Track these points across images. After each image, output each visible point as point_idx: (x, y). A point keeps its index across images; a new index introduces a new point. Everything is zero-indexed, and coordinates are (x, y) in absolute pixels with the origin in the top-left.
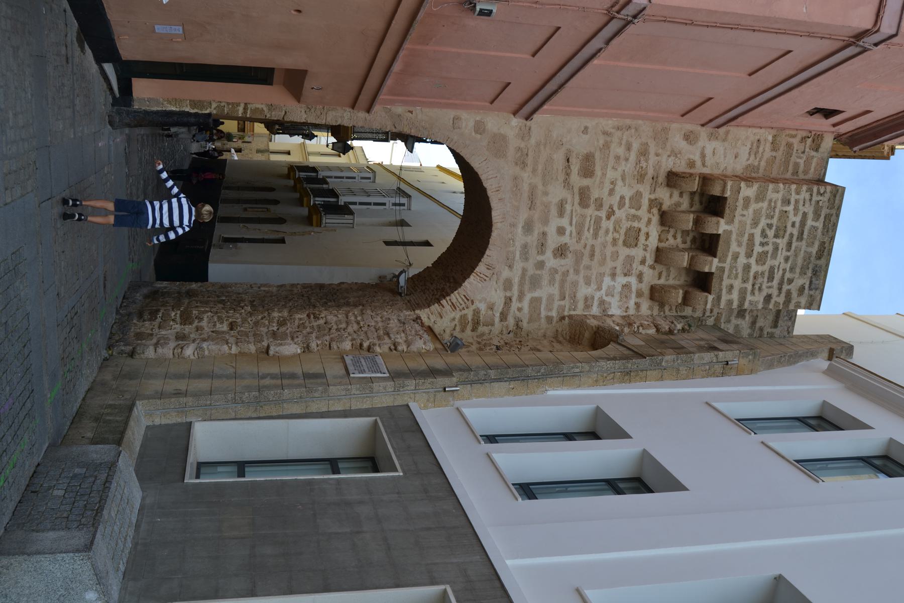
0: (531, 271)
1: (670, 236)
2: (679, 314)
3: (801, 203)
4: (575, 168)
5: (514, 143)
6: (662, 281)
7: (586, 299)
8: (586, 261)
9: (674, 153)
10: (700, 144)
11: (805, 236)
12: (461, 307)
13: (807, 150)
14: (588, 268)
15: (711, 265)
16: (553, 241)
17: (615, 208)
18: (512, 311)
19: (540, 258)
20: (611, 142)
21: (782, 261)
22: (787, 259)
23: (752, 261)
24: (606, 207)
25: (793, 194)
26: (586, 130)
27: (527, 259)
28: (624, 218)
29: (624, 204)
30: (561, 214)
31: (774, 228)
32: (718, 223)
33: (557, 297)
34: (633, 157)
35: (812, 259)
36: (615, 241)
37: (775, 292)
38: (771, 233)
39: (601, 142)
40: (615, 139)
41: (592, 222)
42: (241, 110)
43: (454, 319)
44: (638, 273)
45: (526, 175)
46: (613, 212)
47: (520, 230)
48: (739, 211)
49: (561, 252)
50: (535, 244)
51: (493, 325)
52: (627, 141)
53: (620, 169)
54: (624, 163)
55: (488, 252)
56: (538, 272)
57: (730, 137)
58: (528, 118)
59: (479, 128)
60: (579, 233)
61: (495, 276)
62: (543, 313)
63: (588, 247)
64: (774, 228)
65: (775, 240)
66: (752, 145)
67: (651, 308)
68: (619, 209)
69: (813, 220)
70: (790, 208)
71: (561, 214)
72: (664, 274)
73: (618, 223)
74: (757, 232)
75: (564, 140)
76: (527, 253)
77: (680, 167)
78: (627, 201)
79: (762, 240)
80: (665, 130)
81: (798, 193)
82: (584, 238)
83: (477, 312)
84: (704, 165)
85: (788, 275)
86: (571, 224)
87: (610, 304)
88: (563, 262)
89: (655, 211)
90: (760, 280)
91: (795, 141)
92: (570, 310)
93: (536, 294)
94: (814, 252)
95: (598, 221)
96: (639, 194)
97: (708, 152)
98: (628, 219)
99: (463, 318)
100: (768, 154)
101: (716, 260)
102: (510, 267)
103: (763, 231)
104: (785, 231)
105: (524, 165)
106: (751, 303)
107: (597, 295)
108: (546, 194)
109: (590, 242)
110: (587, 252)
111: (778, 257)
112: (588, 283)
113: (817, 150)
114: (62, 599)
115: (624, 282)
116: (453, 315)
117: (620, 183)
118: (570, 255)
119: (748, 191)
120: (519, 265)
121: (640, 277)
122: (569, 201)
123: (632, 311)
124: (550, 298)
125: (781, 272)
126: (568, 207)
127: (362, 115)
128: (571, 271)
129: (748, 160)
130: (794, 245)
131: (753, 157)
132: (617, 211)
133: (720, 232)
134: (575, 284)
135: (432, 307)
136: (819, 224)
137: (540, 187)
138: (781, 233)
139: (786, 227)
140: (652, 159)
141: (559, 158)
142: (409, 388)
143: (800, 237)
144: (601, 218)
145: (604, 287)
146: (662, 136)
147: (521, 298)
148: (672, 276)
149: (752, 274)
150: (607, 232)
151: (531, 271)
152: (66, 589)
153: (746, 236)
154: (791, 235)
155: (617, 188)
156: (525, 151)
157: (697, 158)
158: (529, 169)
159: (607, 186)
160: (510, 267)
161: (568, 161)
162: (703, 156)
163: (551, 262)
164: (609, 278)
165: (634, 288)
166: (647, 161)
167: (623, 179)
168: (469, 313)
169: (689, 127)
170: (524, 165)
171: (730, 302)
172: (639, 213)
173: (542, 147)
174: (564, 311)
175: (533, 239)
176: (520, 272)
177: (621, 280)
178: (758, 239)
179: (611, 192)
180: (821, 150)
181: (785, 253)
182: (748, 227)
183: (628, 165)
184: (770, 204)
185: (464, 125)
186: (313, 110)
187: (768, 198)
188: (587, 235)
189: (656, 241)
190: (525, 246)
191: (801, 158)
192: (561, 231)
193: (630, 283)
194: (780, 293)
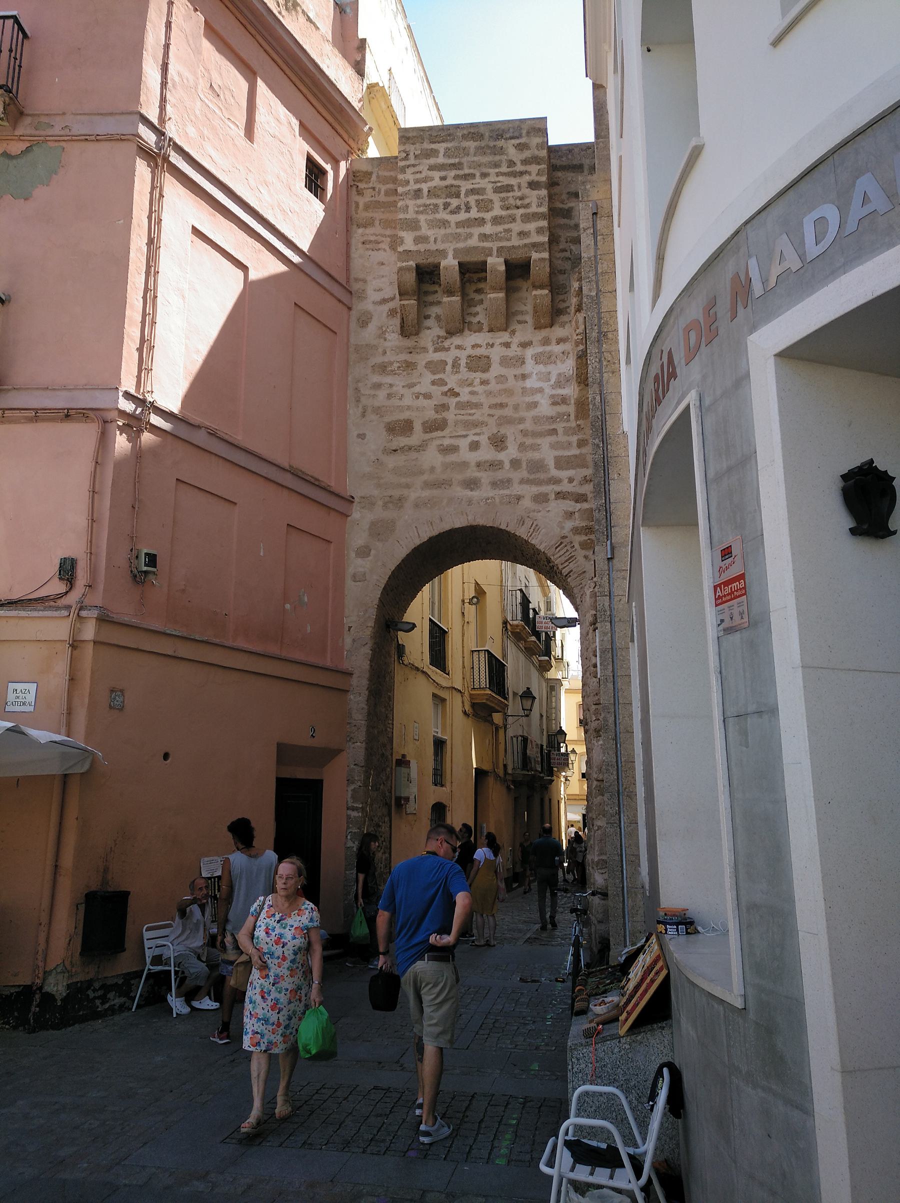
0: (524, 473)
1: (475, 320)
3: (418, 176)
4: (403, 441)
5: (379, 513)
6: (529, 318)
7: (554, 404)
8: (508, 412)
9: (382, 335)
10: (370, 307)
11: (457, 160)
13: (371, 185)
14: (516, 408)
15: (496, 263)
16: (486, 453)
17: (446, 389)
21: (487, 180)
22: (484, 175)
24: (445, 400)
25: (408, 188)
27: (509, 481)
31: (448, 200)
32: (446, 268)
33: (553, 439)
34: (388, 380)
35: (483, 144)
36: (484, 382)
37: (527, 178)
38: (454, 202)
39: (373, 417)
41: (462, 412)
42: (354, 814)
44: (520, 348)
45: (413, 495)
46: (451, 390)
47: (475, 493)
48: (433, 247)
49: (499, 442)
50: (490, 473)
54: (394, 388)
55: (503, 527)
57: (361, 276)
58: (350, 500)
59: (364, 552)
60: (475, 425)
61: (531, 514)
62: (575, 451)
64: (448, 200)
65: (462, 196)
70: (425, 187)
71: (454, 449)
72: (520, 318)
74: (453, 219)
75: (373, 458)
76: (502, 481)
78: (437, 377)
79: (463, 211)
81: (407, 182)
82: (481, 419)
83: (576, 531)
84: (392, 299)
86: (465, 436)
87: (560, 374)
89: (447, 344)
90: (512, 201)
92: (568, 421)
93: (551, 463)
94: (476, 144)
95: (460, 406)
96: (430, 365)
97: (377, 297)
100: (377, 229)
101: (490, 260)
102: (519, 498)
103: (452, 212)
104: (452, 186)
106: (539, 205)
107: (548, 391)
109: (486, 410)
110: (498, 412)
111: (483, 186)
112: (535, 405)
115: (533, 362)
116: (581, 559)
117: (417, 389)
118: (503, 431)
119: (408, 241)
120: (517, 489)
121: (524, 345)
122: (439, 442)
123: (567, 347)
124: (553, 446)
125: (501, 178)
126: (447, 442)
127: (354, 681)
128: (521, 427)
129: (385, 250)
130: (467, 171)
131: (382, 246)
132: (449, 386)
133: (455, 263)
134: (536, 420)
136: (441, 147)
137: (425, 477)
138: (453, 189)
139: (446, 187)
140: (390, 357)
141: (392, 461)
144: (458, 403)
147: (558, 481)
148: (523, 308)
149: (504, 213)
150: (472, 393)
151: (524, 473)
153: (458, 230)
154: (456, 177)
158: (405, 492)
159: (422, 402)
160: (519, 498)
161: (395, 451)
163: (512, 451)
164: (527, 381)
165: (540, 349)
166: (391, 363)
167: (411, 386)
168: (578, 539)
171: (540, 231)
172: (450, 362)
175: (485, 477)
176: (526, 487)
177: (530, 366)
178: (463, 216)
179: (428, 396)
180: (370, 170)
181: (478, 179)
182: (449, 231)
183: (397, 383)
184: (422, 212)
186: (352, 735)
187: (415, 216)
188: (478, 415)
189: (482, 334)
190: (494, 484)
192: (475, 446)
194: (526, 172)
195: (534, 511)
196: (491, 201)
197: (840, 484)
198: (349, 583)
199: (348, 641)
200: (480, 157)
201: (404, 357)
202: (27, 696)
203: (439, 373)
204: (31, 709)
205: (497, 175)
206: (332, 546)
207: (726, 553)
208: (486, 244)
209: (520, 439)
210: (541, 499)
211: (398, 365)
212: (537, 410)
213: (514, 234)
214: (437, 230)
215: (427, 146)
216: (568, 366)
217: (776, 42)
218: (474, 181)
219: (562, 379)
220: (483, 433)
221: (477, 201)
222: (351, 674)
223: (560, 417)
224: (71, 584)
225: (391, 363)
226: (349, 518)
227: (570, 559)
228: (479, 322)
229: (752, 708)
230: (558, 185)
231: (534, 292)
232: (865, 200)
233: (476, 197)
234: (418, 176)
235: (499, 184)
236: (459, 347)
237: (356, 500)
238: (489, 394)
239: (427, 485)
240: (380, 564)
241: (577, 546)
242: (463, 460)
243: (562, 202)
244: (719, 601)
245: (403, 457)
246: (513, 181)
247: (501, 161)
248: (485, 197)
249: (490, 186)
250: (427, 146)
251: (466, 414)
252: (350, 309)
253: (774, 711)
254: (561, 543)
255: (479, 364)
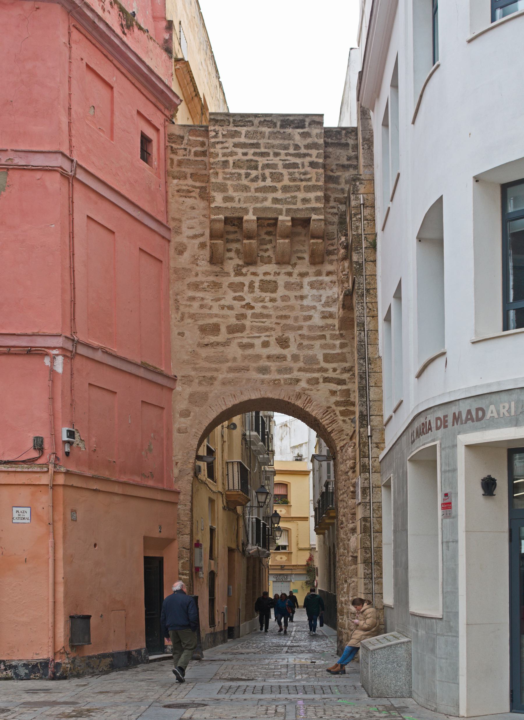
1: (266, 254)
2: (336, 236)
3: (225, 151)
4: (213, 339)
5: (195, 387)
6: (306, 256)
7: (324, 317)
8: (290, 322)
9: (195, 260)
10: (185, 241)
11: (255, 141)
12: (333, 416)
13: (183, 146)
14: (296, 319)
16: (275, 350)
17: (244, 303)
18: (336, 376)
19: (289, 358)
20: (189, 313)
21: (278, 158)
22: (276, 154)
23: (279, 185)
24: (244, 311)
26: (181, 334)
28: (252, 295)
29: (240, 296)
30: (252, 346)
31: (249, 171)
32: (247, 221)
33: (323, 342)
35: (275, 130)
36: (272, 300)
37: (308, 159)
38: (254, 173)
39: (190, 321)
40: (187, 310)
41: (256, 320)
43: (344, 421)
45: (221, 377)
48: (235, 205)
49: (283, 343)
50: (278, 364)
51: (348, 390)
52: (187, 300)
53: (211, 304)
56: (302, 359)
57: (177, 217)
58: (174, 379)
59: (186, 414)
60: (267, 329)
61: (306, 392)
62: (338, 351)
63: (278, 321)
64: (249, 171)
65: (260, 168)
66: (181, 196)
67: (331, 262)
68: (244, 300)
69: (240, 137)
70: (231, 160)
71: (252, 346)
73: (256, 300)
74: (254, 186)
75: (190, 350)
77: (206, 253)
79: (260, 180)
80: (176, 270)
82: (270, 326)
83: (337, 404)
84: (202, 235)
85: (291, 151)
86: (259, 337)
87: (328, 297)
88: (292, 340)
89: (244, 270)
90: (297, 176)
91: (176, 158)
92: (334, 330)
93: (320, 358)
94: (270, 130)
95: (254, 316)
96: (231, 285)
97: (191, 233)
98: (253, 292)
99: (342, 413)
101: (280, 218)
102: (298, 381)
103: (253, 180)
105: (213, 378)
107: (320, 308)
108: (235, 359)
110: (283, 322)
113: (182, 138)
114: (399, 665)
115: (309, 287)
116: (341, 422)
117: (222, 302)
118: (286, 335)
120: (296, 374)
121: (302, 275)
122: (240, 341)
123: (334, 278)
124: (323, 347)
125: (289, 158)
126: (245, 341)
127: (181, 497)
129: (195, 198)
130: (263, 150)
131: (193, 194)
133: (255, 218)
134: (311, 328)
135: (334, 438)
136: (243, 130)
137: (229, 364)
138: (253, 164)
139: (247, 161)
141: (204, 352)
142: (367, 462)
143: (256, 145)
144: (253, 314)
145: (312, 304)
146: (181, 273)
147: (326, 370)
149: (292, 184)
150: (264, 307)
151: (301, 364)
152: (394, 662)
153: (257, 194)
154: (255, 154)
155: (227, 303)
156: (201, 378)
157: (197, 242)
158: (215, 374)
159: (226, 312)
160: (298, 381)
161: (207, 345)
162: (195, 237)
163: (293, 349)
165: (314, 279)
166: (202, 283)
167: (219, 299)
169: (172, 252)
170: (213, 378)
171: (317, 199)
172: (247, 284)
173: (197, 366)
174: (335, 335)
175: (273, 365)
177: (306, 290)
178: (261, 184)
179: (230, 308)
180: (182, 135)
181: (271, 157)
182: (249, 194)
183: (207, 297)
184: (228, 179)
185: (183, 425)
186: (181, 530)
187: (223, 181)
188: (268, 323)
189: (271, 265)
191: (190, 151)
193: (308, 283)
195: (308, 389)
196: (282, 174)
197: (481, 481)
198: (175, 435)
199: (176, 471)
200: (273, 141)
201: (212, 278)
202: (25, 514)
203: (239, 291)
204: (29, 521)
205: (287, 155)
206: (165, 411)
207: (446, 495)
208: (279, 206)
209: (299, 340)
210: (314, 382)
211: (207, 284)
212: (311, 321)
213: (299, 200)
214: (240, 193)
215: (232, 128)
216: (336, 292)
217: (473, 343)
218: (268, 158)
219: (330, 300)
220: (272, 336)
221: (271, 173)
222: (179, 493)
223: (327, 326)
224: (42, 451)
225: (202, 283)
226: (174, 391)
227: (333, 421)
228: (269, 256)
229: (451, 540)
230: (330, 158)
231: (312, 241)
232: (492, 412)
233: (271, 171)
234: (225, 151)
235: (287, 162)
236: (254, 274)
237: (179, 378)
238: (276, 308)
239: (231, 370)
240: (197, 421)
241: (338, 413)
242: (257, 353)
243: (332, 171)
244: (443, 508)
245: (213, 350)
246: (298, 161)
247: (289, 145)
248: (277, 171)
249: (281, 163)
250: (232, 128)
251: (260, 322)
252: (169, 241)
253: (457, 542)
254: (327, 411)
255: (269, 286)
